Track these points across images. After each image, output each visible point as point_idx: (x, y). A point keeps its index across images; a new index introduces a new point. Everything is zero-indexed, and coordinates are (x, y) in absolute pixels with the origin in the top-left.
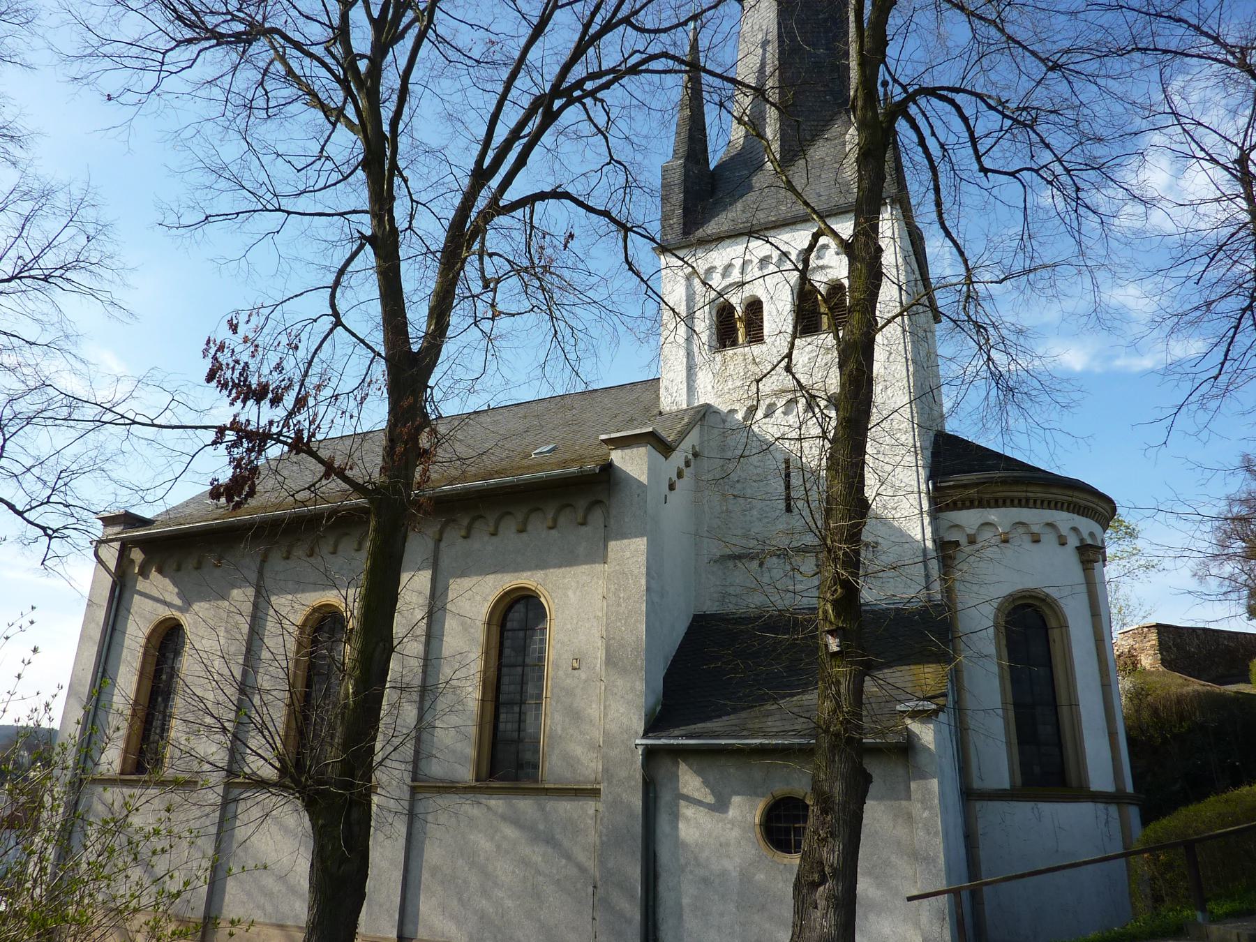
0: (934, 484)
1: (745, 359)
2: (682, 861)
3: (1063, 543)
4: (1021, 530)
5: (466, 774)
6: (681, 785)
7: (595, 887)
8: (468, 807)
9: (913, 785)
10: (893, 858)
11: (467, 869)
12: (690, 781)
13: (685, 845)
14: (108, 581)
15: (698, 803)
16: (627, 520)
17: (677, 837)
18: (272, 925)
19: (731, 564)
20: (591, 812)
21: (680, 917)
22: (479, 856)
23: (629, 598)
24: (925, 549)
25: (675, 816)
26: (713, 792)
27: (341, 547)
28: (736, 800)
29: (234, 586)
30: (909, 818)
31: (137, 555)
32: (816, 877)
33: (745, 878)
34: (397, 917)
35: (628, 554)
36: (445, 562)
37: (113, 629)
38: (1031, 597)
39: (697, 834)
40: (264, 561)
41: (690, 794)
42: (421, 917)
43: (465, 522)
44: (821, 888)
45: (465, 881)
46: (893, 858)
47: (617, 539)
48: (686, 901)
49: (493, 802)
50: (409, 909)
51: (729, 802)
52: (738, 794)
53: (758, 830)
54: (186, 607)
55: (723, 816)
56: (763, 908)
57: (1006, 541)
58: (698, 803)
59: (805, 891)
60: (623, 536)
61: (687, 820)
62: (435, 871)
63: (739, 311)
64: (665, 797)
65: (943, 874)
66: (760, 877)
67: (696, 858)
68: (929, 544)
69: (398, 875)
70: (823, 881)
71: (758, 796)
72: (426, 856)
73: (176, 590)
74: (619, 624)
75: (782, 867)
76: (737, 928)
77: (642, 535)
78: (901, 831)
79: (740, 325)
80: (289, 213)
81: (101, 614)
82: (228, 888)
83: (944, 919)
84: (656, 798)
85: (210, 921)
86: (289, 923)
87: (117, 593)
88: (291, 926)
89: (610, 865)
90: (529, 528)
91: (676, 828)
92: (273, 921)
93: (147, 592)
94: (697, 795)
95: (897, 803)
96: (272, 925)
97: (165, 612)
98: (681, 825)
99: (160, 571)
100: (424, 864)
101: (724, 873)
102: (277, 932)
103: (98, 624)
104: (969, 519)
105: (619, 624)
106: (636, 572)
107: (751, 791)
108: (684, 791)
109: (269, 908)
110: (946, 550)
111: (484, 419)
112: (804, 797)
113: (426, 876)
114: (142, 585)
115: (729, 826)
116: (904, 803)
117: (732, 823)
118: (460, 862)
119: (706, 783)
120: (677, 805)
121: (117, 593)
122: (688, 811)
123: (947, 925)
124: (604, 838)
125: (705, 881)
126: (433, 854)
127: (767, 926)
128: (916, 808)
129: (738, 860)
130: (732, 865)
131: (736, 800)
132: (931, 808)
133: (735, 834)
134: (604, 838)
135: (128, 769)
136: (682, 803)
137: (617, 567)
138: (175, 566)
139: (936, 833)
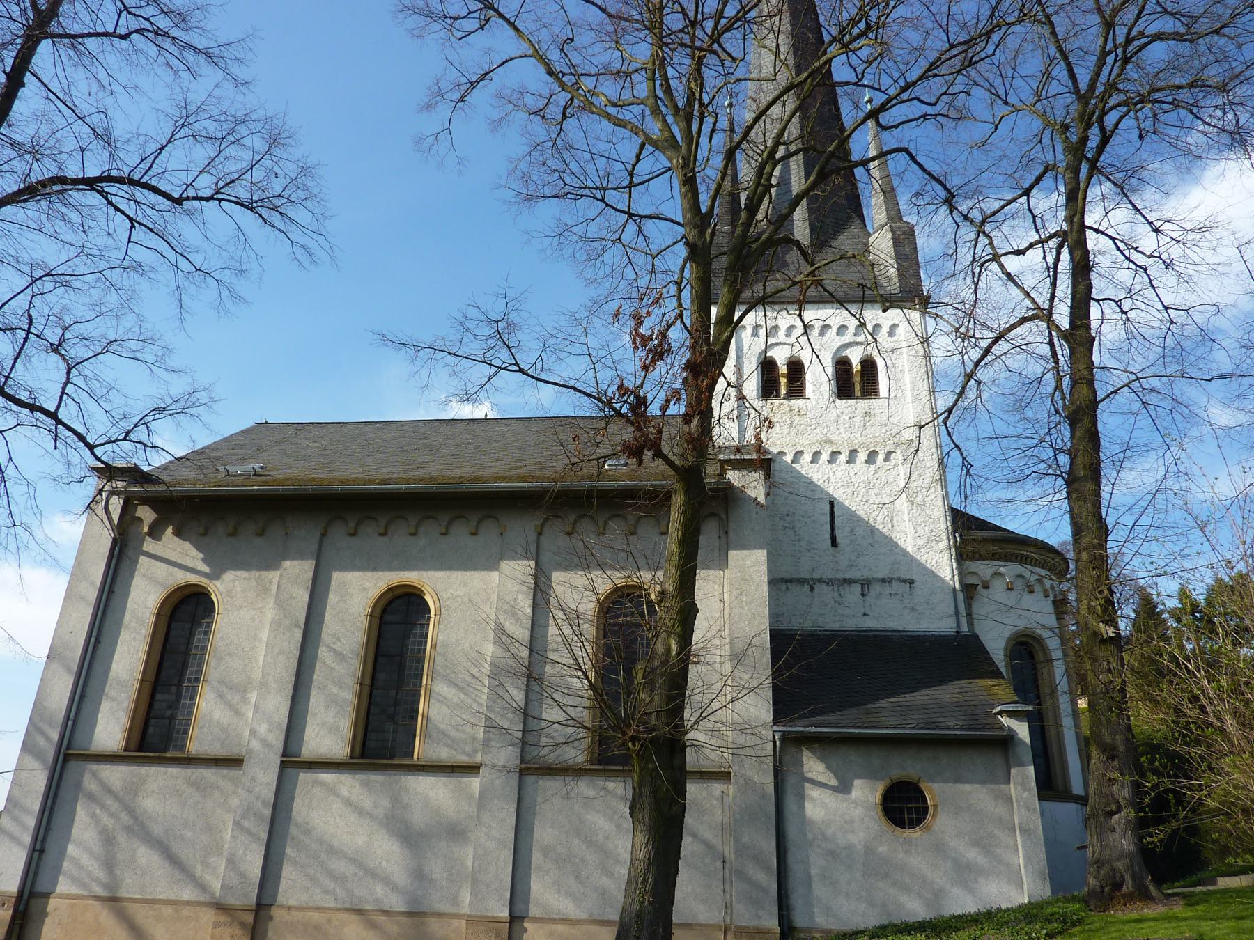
0: (961, 536)
1: (791, 410)
2: (810, 836)
3: (1047, 596)
4: (1020, 580)
5: (577, 755)
6: (805, 770)
7: (724, 862)
8: (585, 788)
9: (1013, 771)
10: (996, 832)
11: (584, 847)
12: (813, 766)
13: (813, 822)
14: (105, 538)
15: (823, 785)
16: (746, 533)
17: (803, 815)
18: (347, 910)
19: (784, 587)
20: (717, 793)
21: (810, 886)
22: (597, 835)
23: (751, 602)
24: (954, 590)
25: (801, 797)
26: (836, 776)
27: (422, 529)
28: (858, 783)
29: (285, 559)
30: (1009, 799)
31: (146, 514)
32: (1114, 807)
33: (869, 851)
34: (508, 896)
35: (748, 563)
36: (546, 557)
37: (111, 591)
38: (1028, 636)
39: (823, 813)
40: (323, 535)
41: (815, 777)
42: (532, 896)
43: (607, 515)
44: (1117, 816)
45: (582, 860)
46: (996, 832)
47: (736, 549)
48: (814, 871)
49: (611, 785)
50: (519, 887)
51: (852, 785)
52: (860, 777)
53: (879, 808)
54: (215, 575)
55: (846, 796)
56: (886, 876)
57: (1011, 589)
58: (823, 785)
59: (1102, 819)
60: (742, 546)
61: (812, 799)
62: (546, 851)
63: (783, 369)
64: (791, 781)
65: (1042, 842)
66: (883, 849)
67: (823, 834)
68: (957, 586)
69: (507, 856)
70: (1119, 811)
71: (877, 779)
72: (536, 836)
73: (201, 555)
74: (742, 624)
75: (902, 840)
76: (864, 894)
77: (761, 548)
78: (1001, 810)
79: (783, 381)
80: (607, 205)
81: (97, 572)
82: (284, 874)
83: (1045, 879)
84: (783, 781)
85: (263, 907)
86: (368, 907)
87: (116, 552)
88: (372, 911)
89: (745, 840)
90: (640, 531)
91: (802, 807)
92: (347, 906)
93: (154, 552)
94: (821, 779)
95: (996, 787)
96: (347, 910)
97: (191, 578)
98: (808, 805)
99: (178, 533)
100: (534, 843)
101: (849, 847)
102: (353, 917)
103: (92, 583)
104: (984, 568)
105: (742, 624)
106: (757, 580)
107: (871, 775)
108: (809, 775)
109: (341, 893)
110: (969, 590)
111: (348, 426)
112: (918, 781)
113: (537, 857)
114: (149, 545)
115: (853, 805)
116: (1003, 786)
117: (855, 802)
118: (576, 842)
119: (829, 768)
120: (803, 787)
121: (116, 552)
122: (813, 792)
123: (1048, 883)
124: (738, 816)
125: (832, 854)
126: (544, 834)
127: (891, 891)
128: (1013, 790)
129: (862, 835)
130: (858, 838)
131: (858, 783)
132: (1029, 790)
133: (858, 812)
134: (738, 816)
135: (133, 745)
136: (807, 785)
137: (739, 574)
138: (201, 530)
139: (1035, 810)
